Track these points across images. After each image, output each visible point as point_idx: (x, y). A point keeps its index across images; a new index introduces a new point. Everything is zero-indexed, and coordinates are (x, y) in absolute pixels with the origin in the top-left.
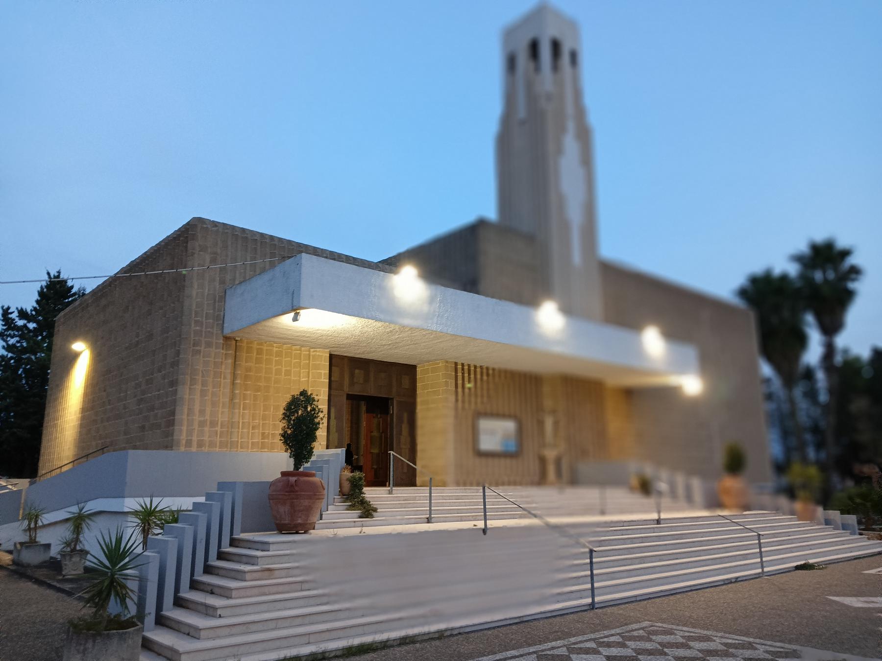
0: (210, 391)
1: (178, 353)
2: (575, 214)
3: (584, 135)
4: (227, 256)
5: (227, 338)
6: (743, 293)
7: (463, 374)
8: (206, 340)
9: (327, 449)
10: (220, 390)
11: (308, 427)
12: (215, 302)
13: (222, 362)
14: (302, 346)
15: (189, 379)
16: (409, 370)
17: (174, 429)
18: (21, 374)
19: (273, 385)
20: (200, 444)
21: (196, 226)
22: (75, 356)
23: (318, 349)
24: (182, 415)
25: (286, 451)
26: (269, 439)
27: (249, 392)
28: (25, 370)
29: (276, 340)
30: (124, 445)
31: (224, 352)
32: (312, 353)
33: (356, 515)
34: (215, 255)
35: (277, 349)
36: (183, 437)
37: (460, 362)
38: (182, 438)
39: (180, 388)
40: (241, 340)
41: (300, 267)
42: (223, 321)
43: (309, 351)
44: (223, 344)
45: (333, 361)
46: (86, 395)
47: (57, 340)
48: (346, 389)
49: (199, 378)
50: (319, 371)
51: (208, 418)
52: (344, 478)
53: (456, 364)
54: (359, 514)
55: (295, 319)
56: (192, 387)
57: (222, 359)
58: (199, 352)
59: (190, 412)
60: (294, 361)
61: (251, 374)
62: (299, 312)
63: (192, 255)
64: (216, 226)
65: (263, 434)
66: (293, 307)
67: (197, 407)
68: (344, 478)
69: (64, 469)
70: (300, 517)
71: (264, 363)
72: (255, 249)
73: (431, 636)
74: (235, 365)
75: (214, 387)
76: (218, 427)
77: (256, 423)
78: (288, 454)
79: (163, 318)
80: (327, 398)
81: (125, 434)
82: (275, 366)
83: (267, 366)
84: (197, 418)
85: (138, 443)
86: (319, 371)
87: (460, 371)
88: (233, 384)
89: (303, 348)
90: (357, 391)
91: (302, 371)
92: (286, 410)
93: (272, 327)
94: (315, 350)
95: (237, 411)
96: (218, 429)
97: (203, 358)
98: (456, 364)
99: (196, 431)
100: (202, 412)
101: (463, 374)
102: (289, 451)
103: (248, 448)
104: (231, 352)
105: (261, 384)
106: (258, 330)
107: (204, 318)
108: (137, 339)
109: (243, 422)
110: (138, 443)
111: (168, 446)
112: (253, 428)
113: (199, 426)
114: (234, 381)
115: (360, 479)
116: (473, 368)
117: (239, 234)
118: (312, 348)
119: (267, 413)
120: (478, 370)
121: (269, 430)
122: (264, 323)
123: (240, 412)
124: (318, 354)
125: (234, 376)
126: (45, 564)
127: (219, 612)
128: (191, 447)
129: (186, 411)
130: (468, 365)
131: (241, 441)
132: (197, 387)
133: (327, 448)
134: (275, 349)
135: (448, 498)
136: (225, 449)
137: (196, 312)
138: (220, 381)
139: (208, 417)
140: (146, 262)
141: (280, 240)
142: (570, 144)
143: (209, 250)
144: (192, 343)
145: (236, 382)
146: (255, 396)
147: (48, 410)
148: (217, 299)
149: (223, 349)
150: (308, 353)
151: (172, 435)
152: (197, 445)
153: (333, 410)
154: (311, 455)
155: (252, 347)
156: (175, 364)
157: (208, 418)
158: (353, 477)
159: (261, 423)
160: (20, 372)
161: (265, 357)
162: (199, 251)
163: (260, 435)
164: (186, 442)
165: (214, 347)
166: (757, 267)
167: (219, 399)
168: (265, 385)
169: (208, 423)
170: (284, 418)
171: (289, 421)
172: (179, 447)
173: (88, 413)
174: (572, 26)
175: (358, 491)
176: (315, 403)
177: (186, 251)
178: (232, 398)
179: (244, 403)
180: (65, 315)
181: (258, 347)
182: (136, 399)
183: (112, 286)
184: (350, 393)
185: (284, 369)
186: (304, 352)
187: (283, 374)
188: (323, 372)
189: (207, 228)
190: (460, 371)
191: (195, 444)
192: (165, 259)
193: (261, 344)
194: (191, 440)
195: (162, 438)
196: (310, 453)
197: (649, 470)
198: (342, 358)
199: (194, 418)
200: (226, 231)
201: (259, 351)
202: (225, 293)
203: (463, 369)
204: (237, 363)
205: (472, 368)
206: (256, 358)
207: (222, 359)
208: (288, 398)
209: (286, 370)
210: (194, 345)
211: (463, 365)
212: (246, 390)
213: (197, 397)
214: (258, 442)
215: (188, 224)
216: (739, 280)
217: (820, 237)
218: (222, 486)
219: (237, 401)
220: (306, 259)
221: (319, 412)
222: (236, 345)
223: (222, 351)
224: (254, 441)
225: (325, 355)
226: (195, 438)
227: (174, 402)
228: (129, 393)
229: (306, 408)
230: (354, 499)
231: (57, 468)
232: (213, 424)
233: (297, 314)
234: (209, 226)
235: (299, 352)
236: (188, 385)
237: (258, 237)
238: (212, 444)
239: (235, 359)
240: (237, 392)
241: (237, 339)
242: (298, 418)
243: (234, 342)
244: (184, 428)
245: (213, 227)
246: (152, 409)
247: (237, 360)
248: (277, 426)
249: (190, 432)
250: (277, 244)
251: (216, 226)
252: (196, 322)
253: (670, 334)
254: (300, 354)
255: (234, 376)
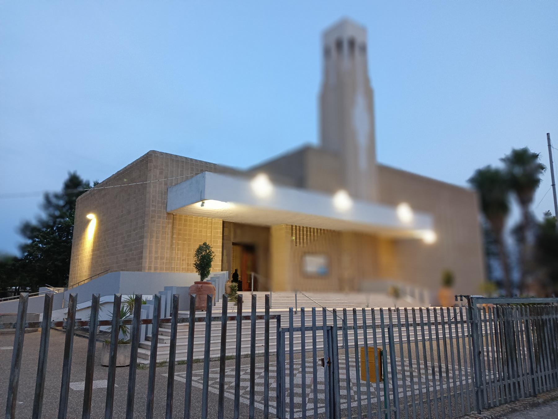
0: (160, 241)
1: (143, 222)
2: (362, 140)
3: (369, 94)
4: (168, 170)
5: (168, 214)
6: (473, 180)
7: (296, 231)
8: (158, 215)
9: (222, 271)
10: (165, 241)
11: (207, 260)
12: (162, 195)
13: (166, 226)
14: (208, 217)
15: (150, 235)
16: (265, 230)
17: (142, 261)
18: (55, 230)
19: (192, 238)
20: (156, 269)
21: (151, 155)
22: (88, 221)
23: (216, 219)
24: (146, 254)
25: (197, 272)
26: (191, 266)
27: (180, 242)
28: (58, 228)
29: (194, 214)
30: (116, 269)
31: (167, 221)
32: (213, 221)
33: (233, 304)
34: (162, 170)
35: (195, 219)
36: (147, 265)
37: (294, 225)
38: (146, 265)
39: (145, 240)
40: (176, 214)
41: (205, 178)
42: (167, 205)
43: (212, 220)
44: (167, 217)
45: (225, 225)
46: (95, 242)
47: (78, 212)
48: (232, 240)
49: (155, 234)
50: (217, 230)
51: (160, 255)
52: (227, 286)
53: (292, 226)
54: (234, 304)
55: (202, 205)
56: (151, 239)
57: (166, 225)
58: (154, 221)
59: (150, 252)
60: (204, 225)
61: (181, 232)
62: (204, 202)
63: (150, 171)
64: (162, 155)
65: (188, 263)
66: (201, 199)
67: (154, 250)
68: (227, 286)
69: (86, 282)
70: (203, 303)
71: (188, 226)
72: (183, 166)
73: (260, 355)
74: (173, 228)
75: (162, 239)
76: (164, 260)
77: (184, 258)
78: (198, 273)
79: (136, 203)
80: (221, 245)
81: (117, 263)
82: (194, 228)
83: (190, 228)
84: (153, 255)
85: (124, 268)
86: (217, 230)
87: (298, 230)
88: (172, 237)
89: (208, 218)
90: (237, 240)
91: (208, 230)
92: (197, 252)
93: (191, 208)
94: (215, 219)
95: (174, 252)
96: (165, 261)
97: (157, 224)
98: (292, 226)
99: (153, 262)
100: (156, 252)
101: (296, 231)
102: (198, 272)
103: (180, 271)
104: (171, 221)
105: (186, 238)
106: (185, 209)
107: (157, 203)
108: (122, 214)
109: (177, 258)
110: (124, 268)
111: (140, 270)
112: (183, 260)
113: (155, 259)
114: (172, 236)
115: (235, 286)
116: (298, 228)
117: (174, 159)
118: (213, 218)
119: (190, 252)
120: (305, 229)
121: (191, 261)
122: (186, 208)
123: (175, 253)
124: (216, 221)
125: (173, 233)
126: (78, 329)
127: (165, 341)
128: (151, 270)
129: (148, 252)
130: (299, 226)
131: (176, 268)
132: (154, 239)
133: (222, 270)
134: (194, 219)
135: (282, 297)
136: (168, 271)
137: (153, 200)
138: (165, 236)
139: (159, 255)
140: (126, 172)
141: (196, 160)
142: (360, 101)
143: (159, 168)
144: (151, 216)
145: (174, 236)
146: (183, 244)
147: (73, 250)
148: (163, 193)
149: (167, 219)
150: (211, 221)
151: (141, 264)
152: (154, 269)
153: (225, 251)
154: (209, 274)
155: (181, 218)
156: (143, 227)
157: (160, 255)
158: (232, 285)
159: (187, 258)
160: (55, 229)
161: (188, 223)
162: (154, 168)
163: (186, 264)
164: (148, 268)
165: (162, 218)
166: (481, 165)
167: (165, 246)
168: (189, 238)
169: (159, 258)
170: (195, 256)
171: (198, 257)
172: (145, 270)
173: (96, 252)
174: (363, 30)
175: (234, 292)
176: (211, 249)
177: (147, 168)
178: (172, 244)
179: (178, 248)
180: (81, 199)
181: (185, 218)
182: (122, 245)
183: (108, 184)
184: (234, 242)
185: (198, 229)
186: (209, 220)
187: (198, 232)
188: (219, 231)
189: (157, 156)
190: (298, 230)
191: (153, 269)
192: (136, 172)
193: (187, 217)
194: (151, 267)
195: (136, 266)
196: (208, 273)
197: (400, 284)
198: (230, 223)
199: (153, 255)
200: (167, 157)
201: (186, 220)
202: (167, 189)
203: (296, 229)
204: (174, 226)
205: (301, 228)
206: (184, 224)
207: (166, 225)
208: (197, 247)
209: (199, 230)
210: (152, 218)
211: (296, 226)
212: (179, 241)
213: (154, 244)
214: (185, 268)
215: (148, 153)
216: (470, 173)
217: (519, 146)
218: (166, 288)
219: (174, 246)
220: (209, 176)
221: (212, 253)
222: (173, 217)
223: (166, 221)
224: (183, 267)
225: (220, 222)
226: (153, 266)
227: (142, 247)
228: (118, 242)
229: (206, 251)
230: (232, 296)
231: (83, 281)
232: (162, 258)
233: (203, 203)
234: (158, 155)
235: (206, 220)
236: (149, 238)
237: (184, 160)
238: (161, 269)
239: (173, 224)
240: (174, 242)
241: (174, 214)
242: (202, 256)
243: (172, 216)
244: (148, 260)
245: (161, 155)
246: (131, 250)
247: (174, 225)
248: (193, 260)
249: (150, 262)
250: (194, 163)
251: (162, 155)
252: (153, 205)
253: (416, 208)
254: (207, 221)
255: (173, 233)
